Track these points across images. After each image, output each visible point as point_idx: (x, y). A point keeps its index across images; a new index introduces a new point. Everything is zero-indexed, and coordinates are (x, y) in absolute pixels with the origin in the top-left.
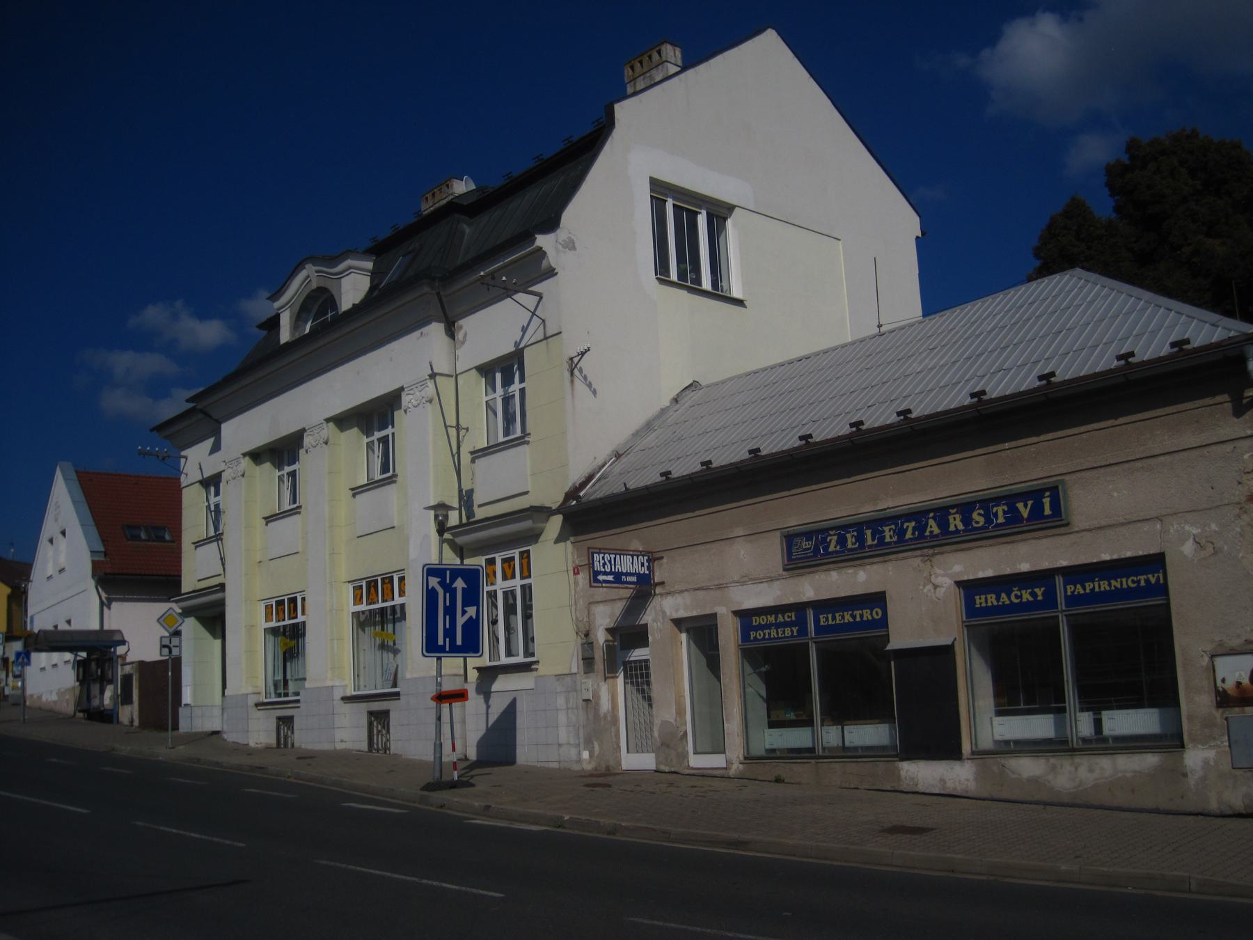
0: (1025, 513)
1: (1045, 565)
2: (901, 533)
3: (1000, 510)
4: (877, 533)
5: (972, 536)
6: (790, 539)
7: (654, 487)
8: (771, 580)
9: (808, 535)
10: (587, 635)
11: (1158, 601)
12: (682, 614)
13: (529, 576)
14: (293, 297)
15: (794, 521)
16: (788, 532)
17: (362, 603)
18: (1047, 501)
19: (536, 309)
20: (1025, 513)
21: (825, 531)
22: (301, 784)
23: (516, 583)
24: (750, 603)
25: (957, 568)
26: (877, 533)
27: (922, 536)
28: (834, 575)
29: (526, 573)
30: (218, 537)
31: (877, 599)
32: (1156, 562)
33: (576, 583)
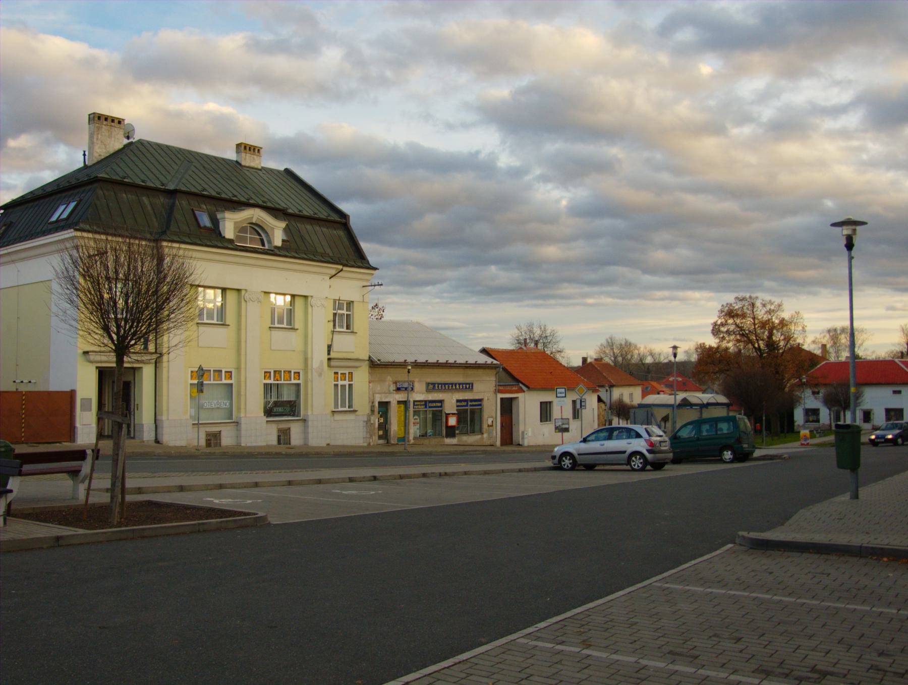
0: (468, 387)
1: (466, 398)
2: (449, 387)
3: (464, 386)
4: (445, 386)
5: (459, 390)
6: (428, 384)
7: (497, 351)
8: (423, 393)
9: (432, 384)
10: (373, 403)
11: (440, 409)
12: (401, 400)
13: (352, 381)
14: (272, 225)
15: (429, 380)
16: (105, 404)
17: (81, 399)
18: (471, 385)
19: (363, 300)
20: (468, 387)
21: (435, 384)
22: (681, 564)
23: (346, 383)
24: (418, 399)
25: (457, 396)
26: (445, 386)
27: (442, 389)
28: (436, 395)
29: (350, 380)
30: (239, 290)
31: (441, 401)
32: (480, 400)
33: (369, 386)
